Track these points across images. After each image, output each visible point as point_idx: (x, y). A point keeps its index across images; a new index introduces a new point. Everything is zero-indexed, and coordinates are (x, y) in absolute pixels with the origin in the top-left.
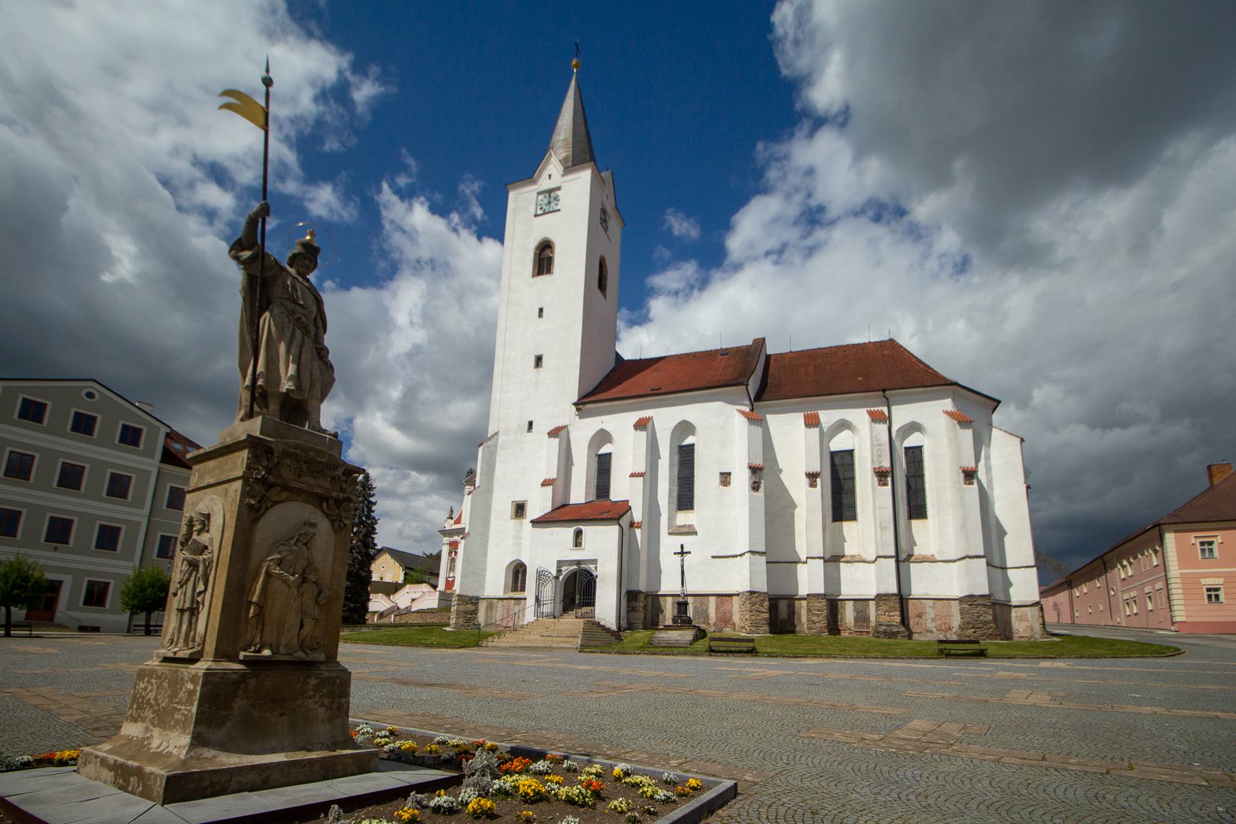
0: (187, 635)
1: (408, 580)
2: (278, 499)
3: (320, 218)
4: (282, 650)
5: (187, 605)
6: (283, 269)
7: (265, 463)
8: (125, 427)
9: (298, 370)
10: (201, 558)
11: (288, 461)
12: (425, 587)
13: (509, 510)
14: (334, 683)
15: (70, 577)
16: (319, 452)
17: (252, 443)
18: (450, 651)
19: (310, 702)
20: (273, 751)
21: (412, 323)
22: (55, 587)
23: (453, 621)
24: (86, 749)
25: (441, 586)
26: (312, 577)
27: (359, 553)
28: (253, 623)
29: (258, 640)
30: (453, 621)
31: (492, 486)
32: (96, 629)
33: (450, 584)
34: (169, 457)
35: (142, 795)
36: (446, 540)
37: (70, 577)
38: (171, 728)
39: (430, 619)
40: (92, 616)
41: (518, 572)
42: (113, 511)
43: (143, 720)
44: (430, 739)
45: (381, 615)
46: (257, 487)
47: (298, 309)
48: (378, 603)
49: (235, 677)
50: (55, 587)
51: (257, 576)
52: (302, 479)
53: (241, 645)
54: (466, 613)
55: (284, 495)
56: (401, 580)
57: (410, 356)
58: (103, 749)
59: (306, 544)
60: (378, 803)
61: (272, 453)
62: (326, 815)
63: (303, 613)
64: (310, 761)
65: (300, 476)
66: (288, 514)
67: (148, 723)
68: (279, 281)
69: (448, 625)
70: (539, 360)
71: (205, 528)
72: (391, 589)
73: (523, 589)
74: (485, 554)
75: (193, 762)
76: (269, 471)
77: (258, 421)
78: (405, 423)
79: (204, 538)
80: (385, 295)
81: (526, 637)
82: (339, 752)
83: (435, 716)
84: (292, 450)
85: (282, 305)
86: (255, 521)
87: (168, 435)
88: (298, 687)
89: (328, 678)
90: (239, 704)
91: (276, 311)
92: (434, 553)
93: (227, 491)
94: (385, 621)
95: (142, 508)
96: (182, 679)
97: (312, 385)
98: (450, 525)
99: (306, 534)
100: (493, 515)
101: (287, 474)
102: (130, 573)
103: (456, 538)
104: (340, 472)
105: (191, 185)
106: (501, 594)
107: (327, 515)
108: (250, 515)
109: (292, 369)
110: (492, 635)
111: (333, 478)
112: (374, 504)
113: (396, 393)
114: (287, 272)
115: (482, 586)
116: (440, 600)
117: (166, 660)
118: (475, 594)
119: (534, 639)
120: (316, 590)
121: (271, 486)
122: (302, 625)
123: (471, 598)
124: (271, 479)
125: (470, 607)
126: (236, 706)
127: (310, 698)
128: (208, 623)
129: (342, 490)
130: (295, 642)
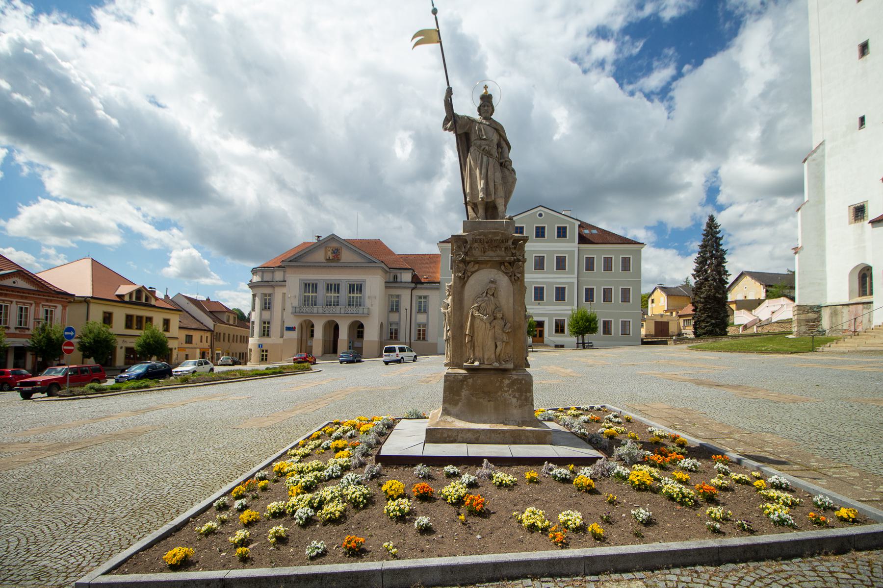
1: (770, 295)
4: (486, 362)
7: (463, 250)
8: (559, 228)
11: (476, 245)
12: (783, 300)
13: (846, 214)
14: (521, 382)
21: (762, 64)
22: (541, 324)
26: (499, 315)
27: (714, 280)
28: (469, 346)
30: (795, 330)
31: (823, 197)
32: (562, 346)
34: (583, 239)
40: (559, 339)
45: (745, 327)
46: (461, 265)
47: (483, 142)
48: (740, 318)
49: (460, 378)
50: (541, 324)
53: (465, 359)
54: (808, 321)
55: (477, 267)
56: (762, 295)
57: (764, 95)
64: (503, 431)
66: (480, 279)
69: (791, 333)
70: (864, 48)
72: (751, 305)
74: (823, 263)
75: (442, 423)
76: (466, 254)
78: (767, 158)
80: (731, 53)
87: (580, 226)
88: (498, 384)
90: (464, 393)
94: (749, 332)
100: (827, 224)
101: (477, 253)
104: (510, 242)
105: (589, 51)
107: (506, 273)
111: (506, 248)
112: (721, 239)
113: (754, 134)
115: (824, 294)
118: (817, 303)
122: (496, 346)
123: (812, 307)
124: (468, 259)
125: (812, 316)
126: (463, 394)
127: (506, 392)
130: (493, 356)
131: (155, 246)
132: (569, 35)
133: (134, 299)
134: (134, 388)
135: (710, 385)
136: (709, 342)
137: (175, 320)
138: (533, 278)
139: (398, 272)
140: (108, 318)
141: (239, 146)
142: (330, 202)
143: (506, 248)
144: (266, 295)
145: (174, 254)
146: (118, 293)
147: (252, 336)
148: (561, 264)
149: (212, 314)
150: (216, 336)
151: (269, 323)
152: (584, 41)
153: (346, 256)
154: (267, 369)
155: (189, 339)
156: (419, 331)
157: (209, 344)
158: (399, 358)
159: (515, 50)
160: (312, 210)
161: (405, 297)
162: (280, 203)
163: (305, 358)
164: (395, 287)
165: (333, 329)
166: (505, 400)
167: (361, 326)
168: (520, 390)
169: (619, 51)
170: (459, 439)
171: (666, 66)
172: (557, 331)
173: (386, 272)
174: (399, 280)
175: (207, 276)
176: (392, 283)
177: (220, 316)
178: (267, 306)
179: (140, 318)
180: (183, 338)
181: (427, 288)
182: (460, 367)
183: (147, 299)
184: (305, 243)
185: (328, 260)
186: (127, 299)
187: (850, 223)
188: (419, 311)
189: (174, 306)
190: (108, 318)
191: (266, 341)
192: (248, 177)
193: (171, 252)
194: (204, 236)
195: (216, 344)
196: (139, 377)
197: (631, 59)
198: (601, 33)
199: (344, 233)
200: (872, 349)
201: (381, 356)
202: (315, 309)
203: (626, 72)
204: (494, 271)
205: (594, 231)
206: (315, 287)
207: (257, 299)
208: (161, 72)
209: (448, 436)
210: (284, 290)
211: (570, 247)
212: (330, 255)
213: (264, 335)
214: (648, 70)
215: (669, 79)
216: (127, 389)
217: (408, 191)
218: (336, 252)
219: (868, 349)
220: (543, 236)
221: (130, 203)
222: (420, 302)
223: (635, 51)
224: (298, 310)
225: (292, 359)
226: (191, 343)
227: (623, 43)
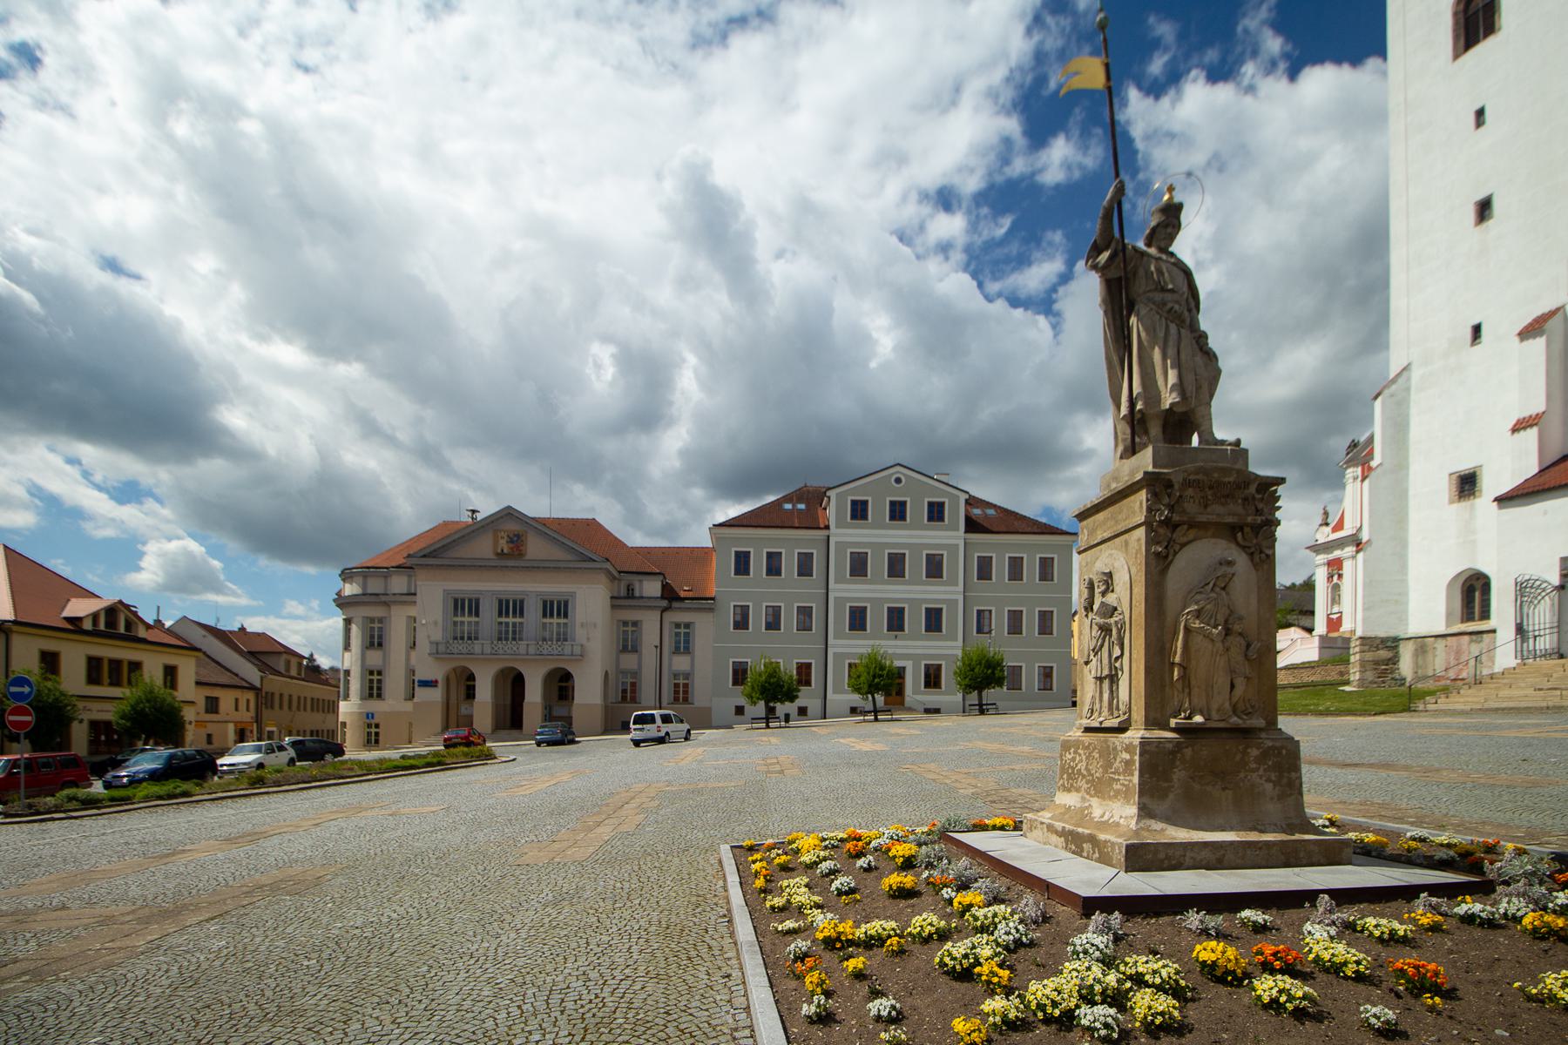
0: (1111, 703)
2: (1184, 540)
3: (1057, 187)
4: (1215, 715)
5: (1106, 672)
6: (1143, 254)
7: (1166, 500)
8: (931, 504)
9: (1180, 377)
10: (1112, 620)
11: (1190, 492)
13: (1444, 487)
16: (1224, 470)
17: (1151, 482)
18: (1360, 719)
22: (901, 673)
23: (1355, 676)
24: (1029, 816)
25: (1320, 627)
26: (1237, 628)
31: (1406, 458)
32: (937, 711)
33: (1334, 624)
34: (972, 526)
35: (1099, 860)
36: (1322, 558)
38: (1110, 798)
39: (1307, 677)
40: (932, 698)
41: (1473, 592)
42: (934, 593)
43: (1078, 790)
44: (1398, 835)
46: (1162, 531)
47: (1168, 296)
49: (1170, 746)
50: (901, 673)
51: (1176, 633)
54: (1377, 663)
55: (1192, 534)
58: (1045, 816)
60: (1371, 902)
62: (1314, 906)
63: (1232, 671)
65: (1206, 507)
66: (1199, 555)
67: (1083, 793)
68: (1141, 272)
69: (1347, 683)
70: (1484, 209)
71: (1109, 586)
73: (1485, 615)
76: (1171, 508)
77: (1148, 453)
79: (1111, 599)
81: (1505, 693)
82: (1297, 837)
83: (1383, 805)
84: (1192, 477)
85: (1149, 299)
86: (1164, 571)
88: (1238, 757)
90: (1178, 775)
91: (1143, 312)
92: (1299, 581)
93: (1127, 543)
96: (1115, 749)
97: (1199, 388)
98: (1325, 535)
99: (1224, 576)
101: (1191, 507)
102: (959, 653)
103: (1337, 553)
104: (1252, 489)
105: (922, 228)
106: (1441, 629)
107: (1244, 548)
108: (1159, 563)
109: (1172, 377)
110: (1432, 693)
111: (1245, 499)
114: (1149, 255)
115: (1403, 618)
116: (1321, 648)
117: (1088, 730)
118: (1392, 633)
119: (1522, 694)
120: (1244, 644)
121: (1175, 527)
122: (1232, 686)
123: (1384, 641)
124: (1176, 518)
125: (1384, 654)
126: (1175, 777)
127: (1253, 771)
128: (1131, 688)
129: (1258, 512)
130: (1227, 705)
131: (109, 533)
132: (890, 199)
133: (102, 626)
134: (160, 798)
135: (1331, 764)
137: (188, 670)
138: (848, 591)
139: (635, 579)
140: (50, 661)
141: (289, 354)
142: (463, 460)
143: (1245, 499)
144: (372, 620)
145: (152, 548)
146: (66, 613)
147: (346, 697)
148: (934, 568)
149: (252, 656)
150: (264, 700)
151: (379, 673)
152: (912, 211)
153: (536, 548)
154: (403, 757)
155: (212, 705)
156: (677, 685)
157: (252, 713)
158: (662, 734)
159: (807, 217)
160: (427, 474)
161: (650, 623)
162: (362, 459)
163: (466, 738)
164: (630, 607)
165: (513, 684)
167: (566, 677)
169: (973, 227)
170: (1188, 861)
171: (1051, 257)
172: (927, 685)
173: (613, 578)
174: (637, 594)
175: (218, 589)
176: (625, 598)
177: (270, 661)
178: (375, 641)
179: (116, 664)
180: (201, 703)
181: (689, 609)
182: (1165, 726)
183: (128, 625)
184: (446, 524)
185: (501, 555)
186: (88, 625)
187: (1451, 502)
188: (677, 651)
189: (180, 641)
190: (50, 661)
191: (375, 706)
192: (289, 406)
193: (144, 543)
194: (210, 515)
195: (266, 713)
196: (154, 776)
197: (990, 245)
198: (945, 199)
199: (535, 506)
200: (1511, 704)
201: (625, 728)
202: (477, 648)
203: (984, 263)
204: (1222, 543)
205: (991, 512)
206: (474, 607)
207: (354, 628)
208: (129, 212)
209: (1168, 857)
210: (412, 611)
211: (949, 537)
212: (503, 545)
213: (371, 695)
214: (1023, 261)
215: (1054, 280)
216: (147, 798)
217: (610, 447)
218: (517, 541)
219: (1504, 705)
220: (903, 518)
221: (51, 449)
222: (677, 634)
223: (1000, 232)
224: (442, 648)
225: (441, 739)
226: (216, 712)
227: (977, 216)
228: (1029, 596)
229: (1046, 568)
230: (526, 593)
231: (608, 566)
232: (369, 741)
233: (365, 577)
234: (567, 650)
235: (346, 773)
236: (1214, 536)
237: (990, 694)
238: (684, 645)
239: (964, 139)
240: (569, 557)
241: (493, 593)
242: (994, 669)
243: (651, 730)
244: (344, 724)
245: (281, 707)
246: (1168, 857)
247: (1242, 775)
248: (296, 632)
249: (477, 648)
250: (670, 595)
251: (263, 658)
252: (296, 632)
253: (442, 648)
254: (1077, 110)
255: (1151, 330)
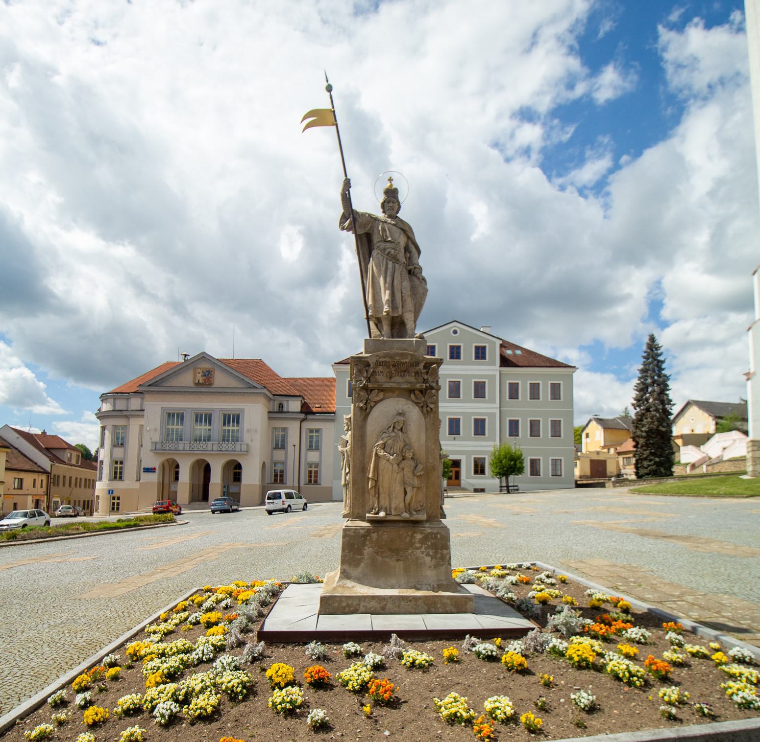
1: (720, 429)
2: (377, 399)
4: (393, 513)
8: (477, 348)
11: (380, 369)
12: (735, 434)
14: (436, 537)
15: (465, 456)
19: (418, 551)
20: (392, 587)
26: (409, 455)
27: (657, 410)
29: (376, 505)
32: (483, 490)
34: (505, 362)
37: (465, 456)
45: (693, 466)
46: (362, 393)
47: (388, 245)
48: (687, 455)
49: (362, 532)
52: (393, 380)
53: (367, 509)
55: (381, 395)
59: (401, 430)
61: (369, 365)
65: (390, 378)
66: (386, 410)
69: (745, 473)
75: (340, 589)
76: (368, 380)
80: (674, 142)
84: (382, 359)
87: (502, 346)
88: (408, 540)
89: (431, 533)
90: (368, 551)
94: (697, 471)
95: (495, 403)
101: (381, 378)
104: (421, 366)
105: (512, 136)
107: (417, 404)
111: (417, 373)
112: (663, 362)
113: (702, 238)
122: (406, 493)
124: (370, 385)
126: (365, 552)
127: (417, 548)
129: (425, 381)
130: (402, 505)
136: (652, 484)
139: (283, 400)
143: (417, 373)
147: (100, 479)
151: (121, 463)
152: (506, 124)
153: (220, 380)
154: (119, 521)
166: (417, 558)
167: (238, 466)
168: (435, 547)
169: (547, 136)
171: (600, 157)
172: (476, 472)
173: (270, 400)
174: (285, 409)
176: (277, 413)
177: (59, 454)
178: (119, 442)
184: (168, 363)
185: (198, 384)
188: (310, 448)
191: (118, 485)
195: (53, 489)
197: (561, 147)
198: (526, 115)
199: (217, 350)
201: (263, 503)
205: (518, 352)
206: (181, 417)
207: (107, 432)
209: (348, 605)
210: (141, 421)
211: (490, 370)
212: (200, 378)
213: (115, 478)
214: (580, 161)
218: (208, 375)
220: (458, 357)
223: (565, 137)
228: (544, 410)
229: (555, 391)
230: (213, 410)
231: (265, 391)
232: (113, 509)
233: (115, 399)
234: (238, 448)
235: (70, 532)
236: (398, 396)
237: (513, 479)
238: (314, 446)
239: (541, 73)
240: (241, 386)
241: (193, 409)
242: (515, 461)
243: (278, 504)
244: (98, 497)
245: (64, 485)
246: (348, 605)
247: (410, 551)
248: (90, 433)
249: (181, 447)
250: (306, 410)
251: (54, 452)
252: (90, 433)
253: (159, 446)
254: (621, 44)
255: (378, 266)
